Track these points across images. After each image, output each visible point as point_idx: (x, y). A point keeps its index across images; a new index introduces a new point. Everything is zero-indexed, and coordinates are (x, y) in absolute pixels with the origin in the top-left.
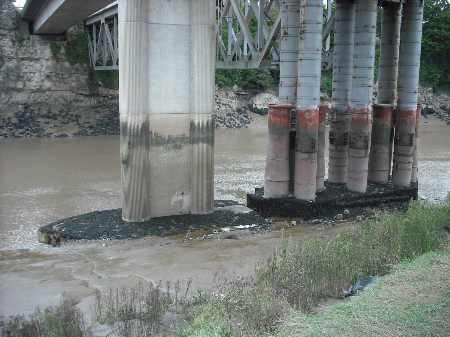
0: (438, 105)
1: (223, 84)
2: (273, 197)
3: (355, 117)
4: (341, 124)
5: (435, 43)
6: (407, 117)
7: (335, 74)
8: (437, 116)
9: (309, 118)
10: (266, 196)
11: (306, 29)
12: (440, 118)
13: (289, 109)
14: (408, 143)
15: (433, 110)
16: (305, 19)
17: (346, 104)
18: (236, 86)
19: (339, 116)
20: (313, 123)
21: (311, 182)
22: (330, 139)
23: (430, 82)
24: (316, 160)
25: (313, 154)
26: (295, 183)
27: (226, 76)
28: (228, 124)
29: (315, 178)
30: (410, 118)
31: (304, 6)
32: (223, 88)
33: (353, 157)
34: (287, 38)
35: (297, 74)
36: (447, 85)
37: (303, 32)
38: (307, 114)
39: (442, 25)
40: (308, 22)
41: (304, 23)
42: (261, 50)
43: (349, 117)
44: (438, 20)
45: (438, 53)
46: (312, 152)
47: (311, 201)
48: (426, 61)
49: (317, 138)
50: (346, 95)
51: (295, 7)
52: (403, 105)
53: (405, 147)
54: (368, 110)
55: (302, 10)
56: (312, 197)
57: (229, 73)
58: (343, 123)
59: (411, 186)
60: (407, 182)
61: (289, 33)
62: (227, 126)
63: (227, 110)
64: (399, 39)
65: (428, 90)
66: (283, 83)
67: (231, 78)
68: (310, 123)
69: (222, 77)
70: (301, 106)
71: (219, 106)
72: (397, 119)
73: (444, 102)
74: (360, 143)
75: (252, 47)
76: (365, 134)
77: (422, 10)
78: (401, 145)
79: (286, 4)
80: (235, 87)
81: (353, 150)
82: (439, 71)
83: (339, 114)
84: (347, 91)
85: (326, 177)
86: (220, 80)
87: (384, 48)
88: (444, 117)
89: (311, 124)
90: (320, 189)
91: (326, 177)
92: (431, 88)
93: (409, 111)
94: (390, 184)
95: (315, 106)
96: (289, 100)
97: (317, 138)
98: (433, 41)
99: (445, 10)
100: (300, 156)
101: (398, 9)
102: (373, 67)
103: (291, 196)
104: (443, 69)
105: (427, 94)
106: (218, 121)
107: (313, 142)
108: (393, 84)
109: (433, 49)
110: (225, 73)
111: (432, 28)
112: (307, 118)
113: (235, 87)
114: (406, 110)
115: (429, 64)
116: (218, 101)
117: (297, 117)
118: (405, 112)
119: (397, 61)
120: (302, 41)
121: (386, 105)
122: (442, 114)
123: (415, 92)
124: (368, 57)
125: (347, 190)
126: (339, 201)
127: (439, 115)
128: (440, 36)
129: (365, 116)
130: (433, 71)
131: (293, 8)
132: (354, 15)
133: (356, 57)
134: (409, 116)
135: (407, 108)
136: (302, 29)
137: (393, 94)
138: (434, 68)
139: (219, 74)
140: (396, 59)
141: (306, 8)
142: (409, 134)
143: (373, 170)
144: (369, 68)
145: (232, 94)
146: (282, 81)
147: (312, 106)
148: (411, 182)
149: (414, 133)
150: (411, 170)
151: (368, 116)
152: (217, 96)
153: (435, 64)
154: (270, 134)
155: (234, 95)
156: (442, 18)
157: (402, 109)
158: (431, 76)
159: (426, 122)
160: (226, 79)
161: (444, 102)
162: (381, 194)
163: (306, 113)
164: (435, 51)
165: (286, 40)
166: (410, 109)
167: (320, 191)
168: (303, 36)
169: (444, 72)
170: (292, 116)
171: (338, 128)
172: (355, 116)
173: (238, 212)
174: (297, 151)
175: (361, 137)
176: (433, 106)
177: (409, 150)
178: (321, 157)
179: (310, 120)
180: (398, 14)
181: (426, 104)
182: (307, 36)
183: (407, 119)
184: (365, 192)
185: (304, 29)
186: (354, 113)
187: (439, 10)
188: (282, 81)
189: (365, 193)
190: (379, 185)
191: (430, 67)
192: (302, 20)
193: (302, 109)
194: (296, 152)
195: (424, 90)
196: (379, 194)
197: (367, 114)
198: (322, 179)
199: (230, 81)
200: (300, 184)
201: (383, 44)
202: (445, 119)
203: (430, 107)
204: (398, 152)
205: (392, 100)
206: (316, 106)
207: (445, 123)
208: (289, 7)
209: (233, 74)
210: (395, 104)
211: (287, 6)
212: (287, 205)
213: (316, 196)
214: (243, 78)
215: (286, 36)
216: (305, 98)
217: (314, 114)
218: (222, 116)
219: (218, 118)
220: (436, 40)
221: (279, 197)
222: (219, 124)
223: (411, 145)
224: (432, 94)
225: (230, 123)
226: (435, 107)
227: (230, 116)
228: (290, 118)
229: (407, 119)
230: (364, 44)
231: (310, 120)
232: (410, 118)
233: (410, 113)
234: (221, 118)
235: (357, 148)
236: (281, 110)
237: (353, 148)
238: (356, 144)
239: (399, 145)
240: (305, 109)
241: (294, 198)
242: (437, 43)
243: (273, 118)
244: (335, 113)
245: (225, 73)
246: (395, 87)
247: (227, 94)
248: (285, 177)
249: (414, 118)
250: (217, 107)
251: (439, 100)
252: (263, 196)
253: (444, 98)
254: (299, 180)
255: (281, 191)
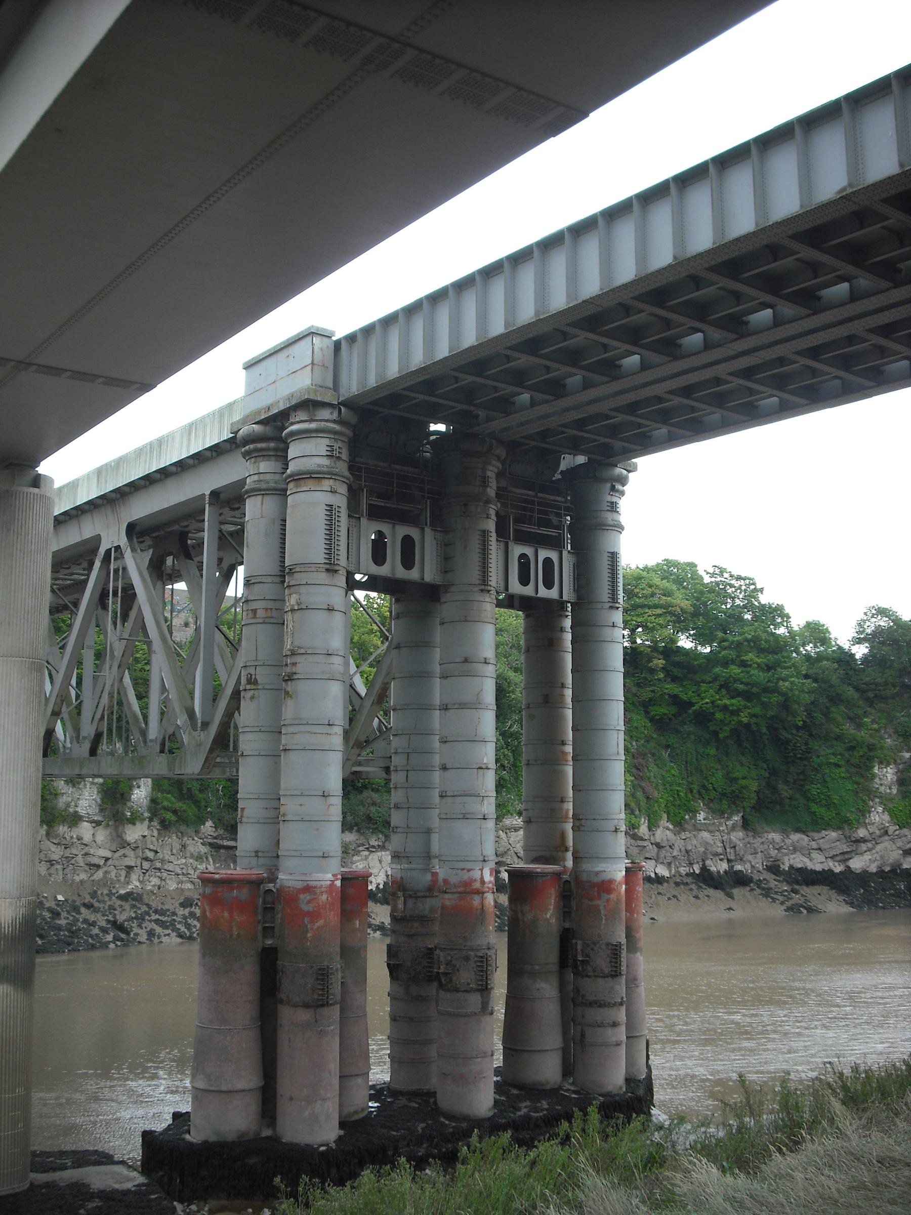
0: (759, 862)
1: (174, 818)
2: (213, 1138)
3: (447, 903)
4: (416, 925)
5: (737, 702)
6: (600, 898)
7: (396, 788)
8: (759, 891)
9: (310, 908)
10: (194, 1137)
11: (298, 669)
12: (766, 895)
13: (255, 884)
14: (607, 971)
15: (746, 876)
16: (296, 643)
17: (427, 870)
18: (209, 824)
19: (410, 902)
20: (321, 922)
21: (322, 1092)
22: (389, 965)
23: (734, 803)
24: (334, 1028)
25: (325, 1011)
26: (278, 1096)
27: (181, 797)
28: (183, 929)
29: (336, 1081)
30: (608, 900)
31: (293, 610)
32: (174, 829)
33: (449, 1014)
34: (256, 692)
35: (279, 789)
36: (778, 807)
37: (290, 678)
38: (304, 897)
39: (750, 656)
40: (302, 651)
41: (293, 653)
42: (205, 725)
43: (435, 902)
44: (739, 644)
45: (747, 726)
46: (323, 1005)
47: (322, 1148)
48: (717, 749)
49: (336, 964)
50: (428, 843)
51: (274, 613)
52: (587, 866)
53: (599, 980)
54: (482, 881)
55: (289, 617)
56: (327, 1134)
57: (189, 790)
58: (423, 919)
59: (627, 1092)
60: (615, 1078)
61: (259, 681)
62: (180, 936)
63: (182, 890)
64: (569, 693)
65: (730, 823)
66: (246, 813)
67: (196, 803)
68: (313, 922)
69: (170, 800)
70: (287, 878)
71: (160, 878)
72: (574, 904)
73: (774, 853)
74: (466, 976)
75: (186, 716)
76: (478, 950)
77: (618, 617)
78: (589, 977)
79: (253, 605)
80: (208, 827)
81: (449, 995)
82: (754, 773)
83: (411, 896)
84: (429, 831)
85: (380, 1073)
86: (165, 808)
87: (531, 717)
88: (776, 893)
89: (318, 924)
90: (356, 1112)
91: (380, 1073)
92: (737, 818)
93: (603, 882)
94: (568, 1086)
95: (327, 876)
96: (261, 861)
97: (336, 964)
98: (733, 698)
99: (755, 618)
100: (291, 1017)
101: (561, 615)
102: (492, 765)
103: (266, 1132)
104: (765, 766)
105: (729, 833)
106: (157, 921)
107: (323, 975)
108: (561, 809)
109: (735, 718)
110: (181, 790)
111: (726, 664)
112: (306, 908)
113: (208, 827)
114: (596, 880)
115: (727, 754)
116: (158, 865)
117: (279, 907)
118: (594, 885)
119: (569, 749)
120: (289, 702)
121: (539, 867)
122: (773, 884)
123: (616, 830)
124: (476, 740)
125: (437, 1111)
126: (408, 1145)
127: (763, 889)
128: (747, 684)
129: (476, 900)
130: (740, 772)
131: (269, 614)
132: (438, 635)
133: (444, 741)
134: (605, 896)
135: (597, 873)
136: (289, 670)
137: (563, 836)
138: (742, 764)
139: (163, 791)
140: (563, 743)
141: (297, 615)
142: (608, 944)
143: (516, 1050)
144: (481, 768)
145: (196, 846)
146: (243, 809)
147: (320, 876)
148: (628, 1080)
149: (623, 941)
150: (624, 1046)
151: (483, 899)
152: (156, 852)
153: (743, 754)
154: (204, 956)
155: (204, 849)
156: (748, 641)
157: (584, 877)
158: (735, 787)
159: (730, 909)
160: (180, 805)
161: (774, 853)
162: (537, 1118)
163: (302, 896)
164: (740, 722)
165: (252, 698)
166: (606, 877)
167: (356, 1117)
168: (290, 687)
169: (767, 775)
170: (264, 903)
171: (410, 936)
172: (449, 900)
173: (102, 1188)
174: (281, 1001)
175: (467, 958)
176: (748, 866)
177: (612, 988)
178: (351, 1016)
179: (314, 916)
180: (562, 630)
181: (729, 861)
182: (302, 687)
183: (599, 902)
184: (491, 1114)
185: (294, 670)
186: (446, 892)
187: (740, 619)
188: (243, 809)
189: (489, 1119)
190: (534, 1092)
191: (730, 763)
192: (288, 645)
193: (290, 884)
194: (280, 1006)
195: (721, 824)
196: (530, 1118)
197: (480, 893)
198: (359, 1080)
199: (191, 811)
200: (291, 1099)
201: (528, 707)
202: (781, 898)
203: (738, 867)
204: (583, 996)
205: (560, 854)
206: (329, 876)
207: (778, 911)
208: (260, 613)
209: (201, 791)
210: (569, 863)
211: (254, 611)
212: (252, 1161)
213: (342, 1133)
214: (228, 802)
215: (253, 687)
216: (298, 854)
217: (324, 897)
218: (166, 907)
219: (156, 912)
220: (739, 694)
221: (231, 1137)
222: (158, 930)
223: (615, 974)
224: (740, 834)
225: (188, 926)
226: (753, 867)
227: (191, 906)
228: (260, 910)
229: (601, 903)
230: (462, 706)
231: (314, 916)
232: (608, 900)
233: (606, 886)
234: (162, 912)
235: (457, 990)
236: (232, 889)
237: (448, 990)
238: (454, 978)
239: (582, 976)
240: (299, 885)
241: (275, 1139)
242: (743, 703)
243: (211, 911)
244: (400, 894)
245: (181, 790)
246: (567, 817)
247: (184, 846)
248: (247, 1078)
249: (618, 901)
250: (155, 881)
251: (761, 848)
252: (187, 1137)
253: (773, 842)
254: (288, 1085)
255: (237, 1119)
